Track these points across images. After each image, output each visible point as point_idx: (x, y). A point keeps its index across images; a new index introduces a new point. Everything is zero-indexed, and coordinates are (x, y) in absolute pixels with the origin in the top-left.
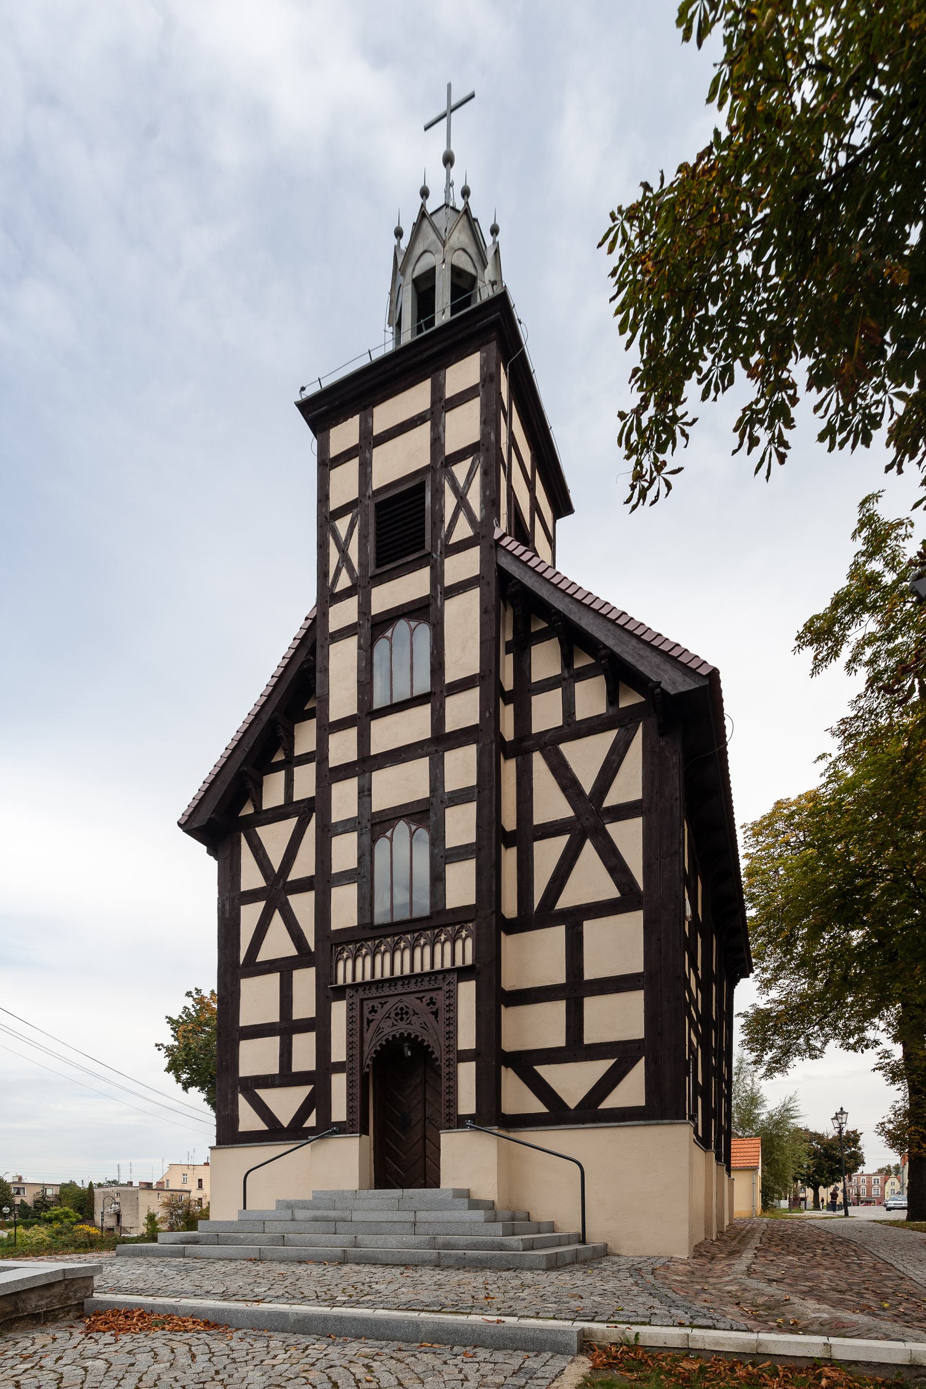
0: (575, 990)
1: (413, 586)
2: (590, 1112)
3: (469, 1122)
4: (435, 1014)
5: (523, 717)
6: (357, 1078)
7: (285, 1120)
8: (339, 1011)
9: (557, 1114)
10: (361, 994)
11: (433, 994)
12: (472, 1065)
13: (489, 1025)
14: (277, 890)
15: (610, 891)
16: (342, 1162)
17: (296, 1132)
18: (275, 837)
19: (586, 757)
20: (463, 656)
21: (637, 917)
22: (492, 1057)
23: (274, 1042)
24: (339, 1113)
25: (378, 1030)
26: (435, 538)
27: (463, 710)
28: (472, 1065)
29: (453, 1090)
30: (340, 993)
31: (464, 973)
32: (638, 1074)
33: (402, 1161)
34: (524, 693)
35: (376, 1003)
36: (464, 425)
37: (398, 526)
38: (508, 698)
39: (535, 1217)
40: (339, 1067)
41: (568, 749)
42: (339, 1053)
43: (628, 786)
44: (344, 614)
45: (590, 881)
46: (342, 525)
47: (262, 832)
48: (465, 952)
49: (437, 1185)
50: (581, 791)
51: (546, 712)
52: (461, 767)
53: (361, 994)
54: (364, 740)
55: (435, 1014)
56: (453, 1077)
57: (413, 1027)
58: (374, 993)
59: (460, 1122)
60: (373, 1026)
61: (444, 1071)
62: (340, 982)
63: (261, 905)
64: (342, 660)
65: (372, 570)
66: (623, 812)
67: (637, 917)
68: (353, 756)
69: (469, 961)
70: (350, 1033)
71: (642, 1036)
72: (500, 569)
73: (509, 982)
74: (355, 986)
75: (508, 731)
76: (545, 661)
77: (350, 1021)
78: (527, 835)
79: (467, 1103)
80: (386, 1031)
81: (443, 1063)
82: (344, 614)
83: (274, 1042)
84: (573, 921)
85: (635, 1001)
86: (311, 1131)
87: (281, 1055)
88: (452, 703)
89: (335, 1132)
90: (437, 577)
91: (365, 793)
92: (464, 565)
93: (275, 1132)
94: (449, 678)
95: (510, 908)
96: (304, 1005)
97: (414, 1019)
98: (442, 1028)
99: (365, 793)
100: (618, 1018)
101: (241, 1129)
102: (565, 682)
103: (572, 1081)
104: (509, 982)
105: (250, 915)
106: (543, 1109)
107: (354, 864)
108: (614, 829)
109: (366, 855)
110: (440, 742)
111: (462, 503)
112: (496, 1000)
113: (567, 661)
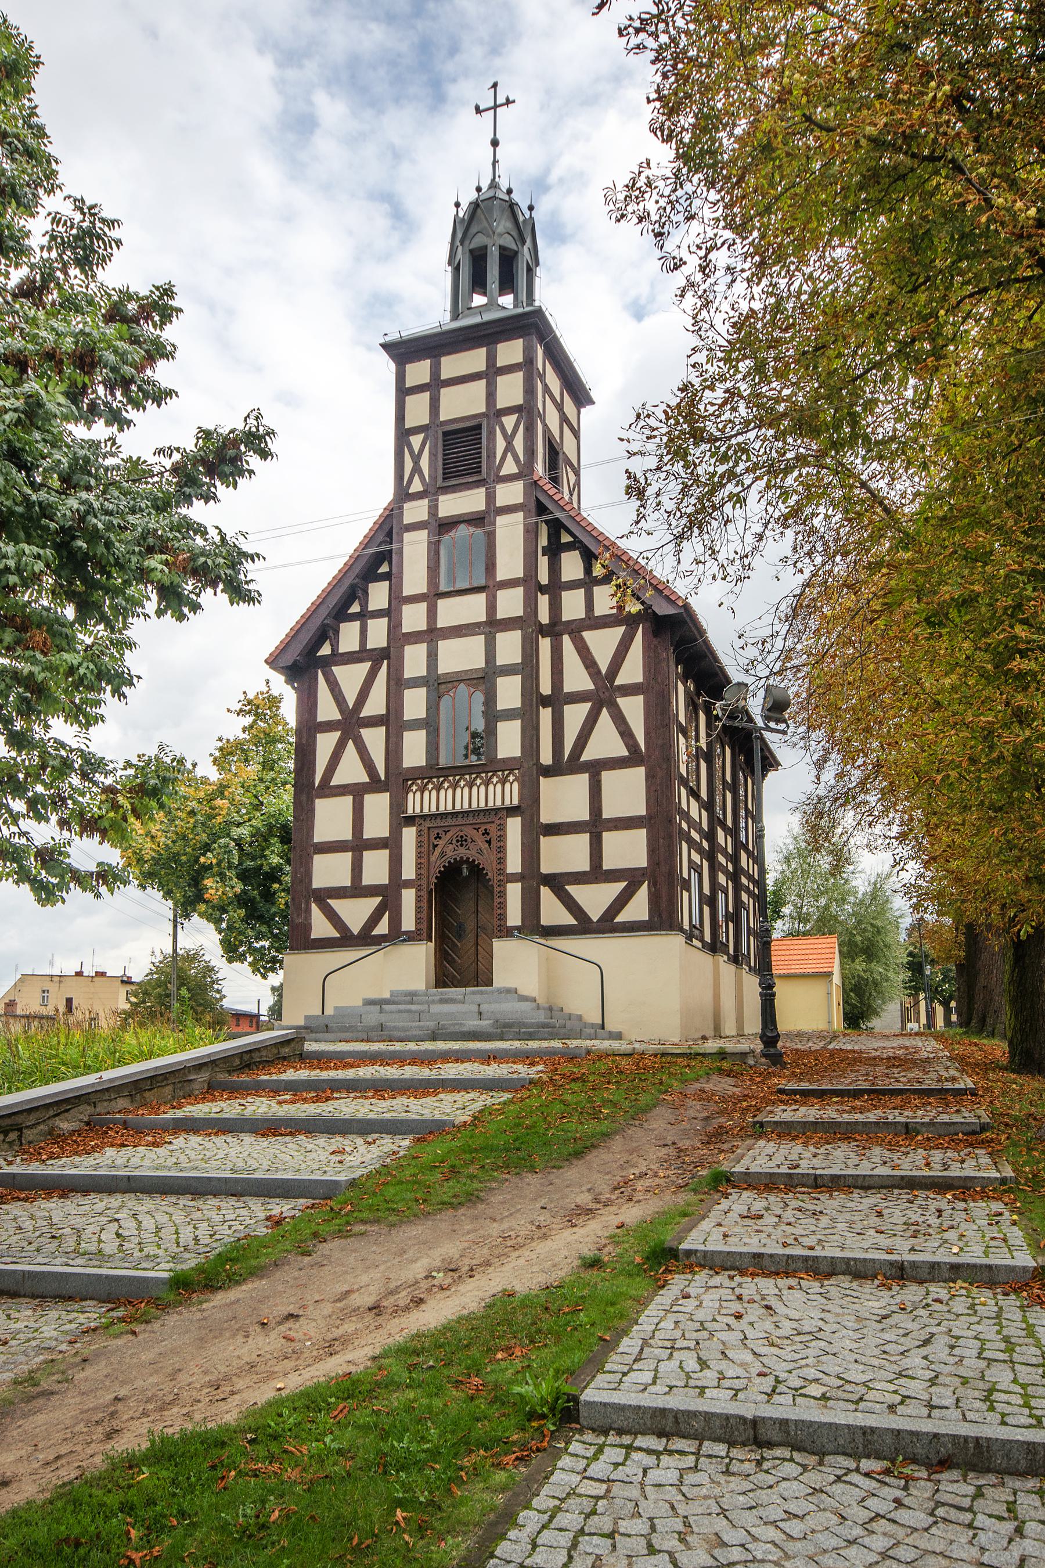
0: (596, 826)
1: (472, 501)
2: (608, 924)
3: (516, 933)
4: (489, 842)
5: (555, 607)
6: (424, 894)
7: (355, 927)
8: (409, 835)
9: (584, 926)
10: (432, 825)
11: (487, 827)
12: (518, 886)
13: (531, 853)
14: (351, 724)
15: (621, 750)
16: (411, 966)
17: (366, 939)
18: (350, 677)
19: (603, 643)
20: (510, 562)
21: (641, 771)
22: (534, 878)
23: (583, 840)
24: (408, 923)
25: (443, 854)
26: (489, 468)
27: (511, 603)
28: (518, 886)
29: (503, 906)
30: (410, 821)
31: (512, 811)
32: (642, 897)
33: (460, 964)
34: (555, 588)
35: (440, 831)
36: (510, 390)
37: (462, 452)
38: (542, 589)
39: (566, 1010)
40: (408, 884)
41: (590, 637)
42: (409, 872)
43: (632, 671)
44: (416, 511)
45: (606, 742)
46: (416, 441)
47: (339, 671)
48: (511, 794)
49: (489, 983)
50: (599, 672)
51: (573, 605)
52: (509, 647)
53: (428, 824)
54: (432, 614)
55: (489, 842)
56: (503, 894)
57: (471, 853)
58: (439, 822)
59: (509, 933)
60: (438, 850)
61: (497, 889)
62: (410, 811)
63: (337, 734)
64: (414, 550)
65: (440, 482)
66: (629, 690)
67: (641, 771)
68: (423, 626)
69: (516, 802)
70: (419, 855)
71: (645, 865)
72: (538, 500)
73: (546, 817)
74: (424, 817)
75: (544, 618)
76: (572, 566)
77: (419, 845)
78: (558, 700)
79: (514, 917)
80: (450, 854)
81: (495, 883)
82: (416, 511)
83: (583, 840)
84: (596, 769)
85: (641, 835)
86: (381, 939)
87: (353, 870)
88: (502, 595)
89: (405, 940)
90: (491, 497)
91: (432, 657)
92: (511, 493)
93: (346, 939)
94: (426, 395)
95: (546, 757)
96: (377, 825)
97: (471, 846)
98: (493, 857)
99: (432, 657)
100: (628, 850)
101: (314, 935)
102: (589, 583)
103: (595, 899)
104: (546, 817)
105: (325, 743)
106: (574, 922)
107: (423, 714)
108: (622, 702)
109: (433, 706)
110: (493, 626)
111: (509, 448)
112: (536, 831)
113: (588, 570)
